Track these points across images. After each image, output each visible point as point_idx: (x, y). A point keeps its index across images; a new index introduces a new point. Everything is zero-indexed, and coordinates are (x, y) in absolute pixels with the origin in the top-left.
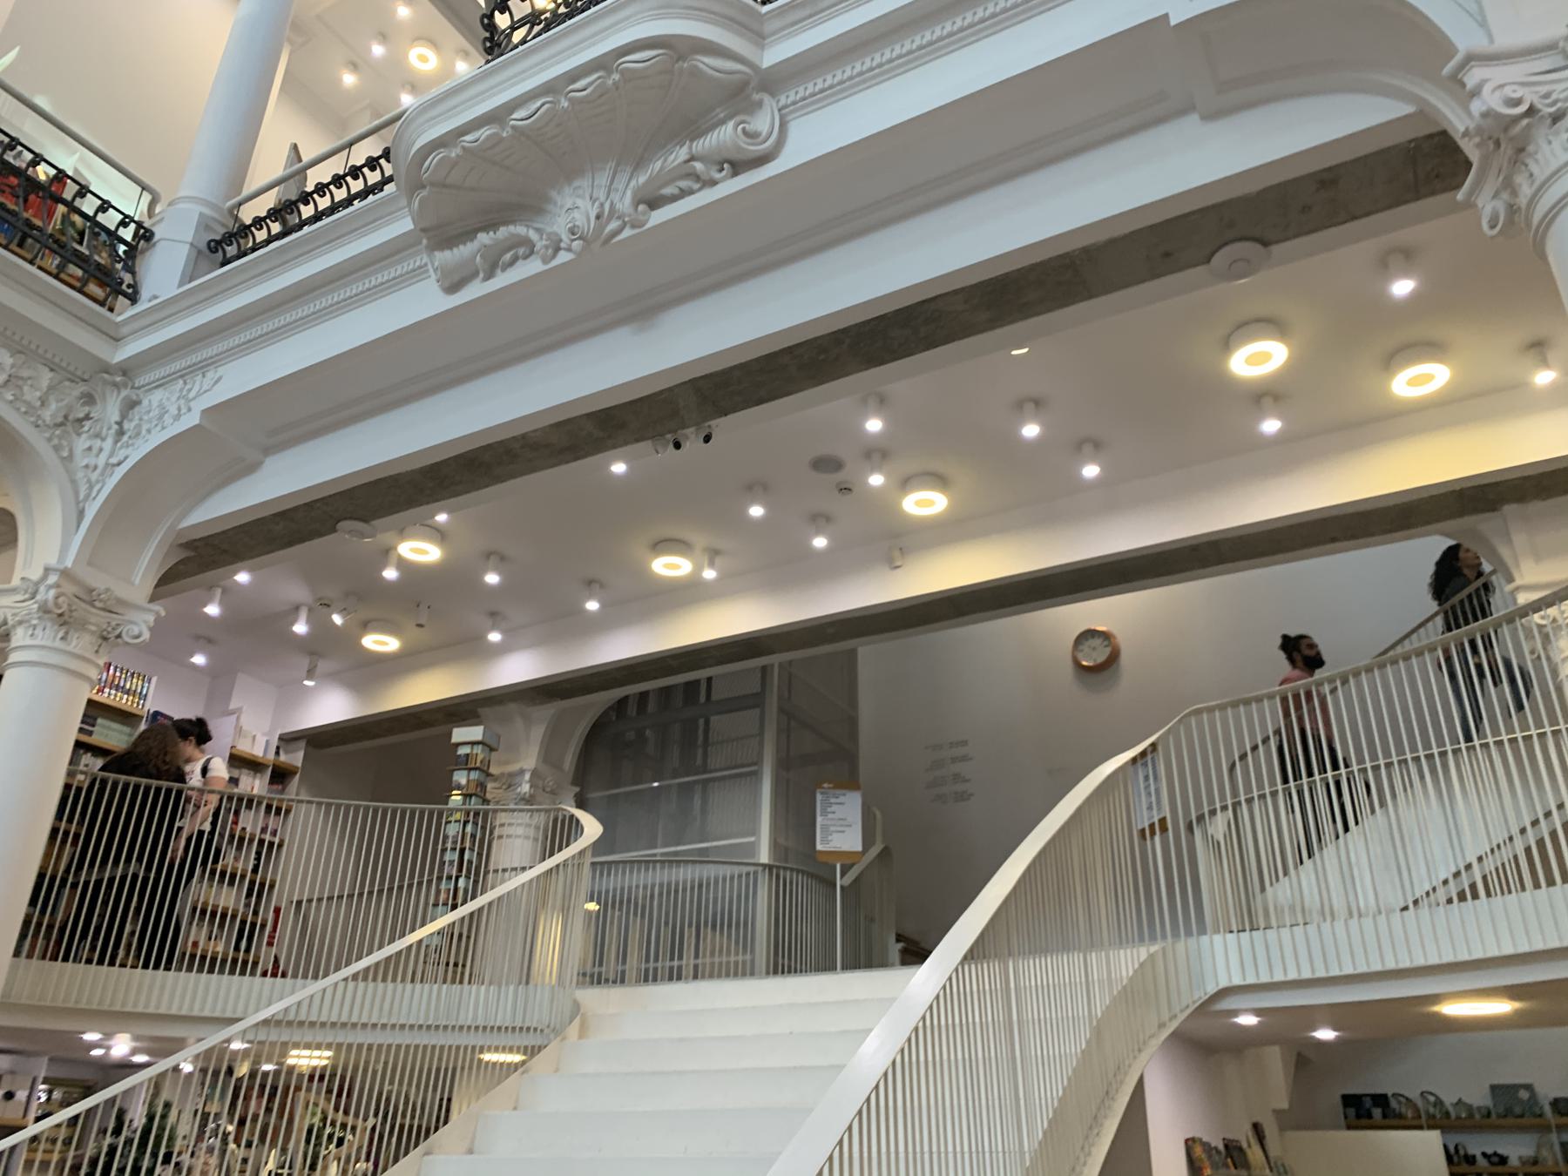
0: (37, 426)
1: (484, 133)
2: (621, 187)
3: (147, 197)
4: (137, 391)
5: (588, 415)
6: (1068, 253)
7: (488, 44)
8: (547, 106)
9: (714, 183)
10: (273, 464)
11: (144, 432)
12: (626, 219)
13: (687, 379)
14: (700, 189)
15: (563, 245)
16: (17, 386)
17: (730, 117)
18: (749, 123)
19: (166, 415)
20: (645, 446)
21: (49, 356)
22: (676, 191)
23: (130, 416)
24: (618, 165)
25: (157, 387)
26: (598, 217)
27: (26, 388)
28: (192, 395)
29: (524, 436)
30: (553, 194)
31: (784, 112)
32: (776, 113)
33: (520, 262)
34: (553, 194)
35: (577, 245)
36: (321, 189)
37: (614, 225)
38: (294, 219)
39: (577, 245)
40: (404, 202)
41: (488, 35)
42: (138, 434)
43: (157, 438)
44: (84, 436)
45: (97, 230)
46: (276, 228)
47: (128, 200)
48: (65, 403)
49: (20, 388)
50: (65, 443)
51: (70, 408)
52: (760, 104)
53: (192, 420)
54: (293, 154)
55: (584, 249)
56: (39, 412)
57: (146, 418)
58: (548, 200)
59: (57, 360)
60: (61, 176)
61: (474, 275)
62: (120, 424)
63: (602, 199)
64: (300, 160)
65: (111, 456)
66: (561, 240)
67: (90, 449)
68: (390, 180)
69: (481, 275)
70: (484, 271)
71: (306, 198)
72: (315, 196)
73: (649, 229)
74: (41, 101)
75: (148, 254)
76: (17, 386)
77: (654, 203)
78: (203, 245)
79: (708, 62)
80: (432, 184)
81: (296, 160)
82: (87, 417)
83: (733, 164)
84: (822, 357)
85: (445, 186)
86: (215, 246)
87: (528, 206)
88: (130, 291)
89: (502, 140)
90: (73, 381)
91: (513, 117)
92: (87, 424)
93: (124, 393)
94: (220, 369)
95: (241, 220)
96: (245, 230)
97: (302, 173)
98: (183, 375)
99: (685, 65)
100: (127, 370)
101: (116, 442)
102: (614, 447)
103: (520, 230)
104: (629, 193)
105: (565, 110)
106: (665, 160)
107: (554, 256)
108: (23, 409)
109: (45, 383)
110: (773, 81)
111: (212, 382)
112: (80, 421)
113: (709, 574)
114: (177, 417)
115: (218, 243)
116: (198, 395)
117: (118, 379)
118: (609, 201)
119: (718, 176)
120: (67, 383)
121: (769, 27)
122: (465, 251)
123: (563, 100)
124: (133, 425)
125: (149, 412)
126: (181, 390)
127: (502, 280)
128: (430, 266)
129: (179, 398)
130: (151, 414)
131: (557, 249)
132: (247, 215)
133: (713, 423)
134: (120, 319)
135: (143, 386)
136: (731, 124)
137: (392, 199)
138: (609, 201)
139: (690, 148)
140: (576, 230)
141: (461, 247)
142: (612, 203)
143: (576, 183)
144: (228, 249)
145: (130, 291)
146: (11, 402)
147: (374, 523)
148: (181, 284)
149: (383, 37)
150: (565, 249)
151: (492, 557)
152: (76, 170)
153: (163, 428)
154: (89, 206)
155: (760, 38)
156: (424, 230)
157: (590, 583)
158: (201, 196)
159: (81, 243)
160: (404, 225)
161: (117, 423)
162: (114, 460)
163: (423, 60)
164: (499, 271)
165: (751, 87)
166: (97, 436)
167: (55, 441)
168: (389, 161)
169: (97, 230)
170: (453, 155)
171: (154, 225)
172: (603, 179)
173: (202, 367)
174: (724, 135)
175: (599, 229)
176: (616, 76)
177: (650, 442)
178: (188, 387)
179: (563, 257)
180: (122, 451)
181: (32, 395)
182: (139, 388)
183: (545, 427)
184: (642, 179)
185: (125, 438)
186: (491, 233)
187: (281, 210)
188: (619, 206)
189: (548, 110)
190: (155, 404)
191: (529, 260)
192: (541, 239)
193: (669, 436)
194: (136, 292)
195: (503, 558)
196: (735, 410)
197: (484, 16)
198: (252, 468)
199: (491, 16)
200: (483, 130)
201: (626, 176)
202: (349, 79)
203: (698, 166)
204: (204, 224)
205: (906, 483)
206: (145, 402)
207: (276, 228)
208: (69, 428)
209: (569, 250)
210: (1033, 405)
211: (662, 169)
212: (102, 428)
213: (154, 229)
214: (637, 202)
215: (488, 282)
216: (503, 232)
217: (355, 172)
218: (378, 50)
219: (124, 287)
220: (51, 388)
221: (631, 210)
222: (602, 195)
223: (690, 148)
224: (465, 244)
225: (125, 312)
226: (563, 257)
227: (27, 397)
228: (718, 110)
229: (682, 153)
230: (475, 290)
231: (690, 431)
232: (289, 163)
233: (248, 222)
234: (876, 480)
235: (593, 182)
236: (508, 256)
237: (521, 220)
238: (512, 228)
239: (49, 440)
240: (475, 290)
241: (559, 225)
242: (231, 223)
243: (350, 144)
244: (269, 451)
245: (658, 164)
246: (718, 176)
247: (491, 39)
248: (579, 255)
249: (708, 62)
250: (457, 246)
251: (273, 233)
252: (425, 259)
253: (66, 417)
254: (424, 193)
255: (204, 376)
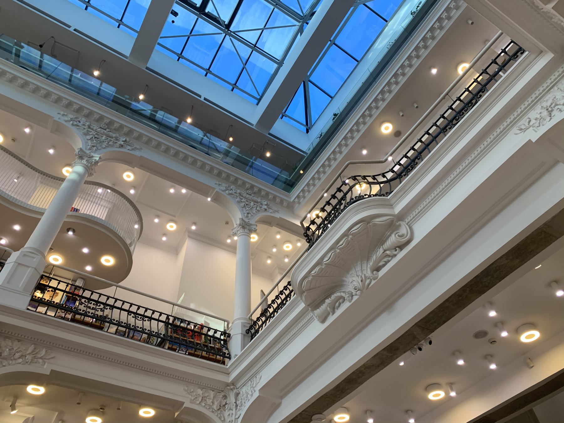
0: (213, 412)
1: (317, 269)
2: (365, 268)
3: (226, 323)
4: (238, 389)
5: (384, 349)
6: (538, 228)
7: (308, 240)
8: (333, 253)
9: (395, 255)
10: (285, 401)
11: (243, 403)
12: (371, 278)
13: (414, 324)
14: (391, 259)
15: (353, 294)
16: (205, 400)
17: (392, 233)
18: (399, 233)
19: (249, 395)
20: (408, 353)
21: (211, 386)
22: (384, 263)
23: (238, 399)
24: (361, 262)
25: (243, 386)
26: (362, 281)
27: (207, 400)
28: (254, 385)
29: (364, 365)
30: (344, 279)
31: (409, 224)
32: (406, 225)
33: (342, 305)
34: (344, 279)
35: (358, 293)
36: (273, 302)
37: (368, 281)
38: (268, 314)
39: (358, 293)
40: (299, 298)
41: (307, 238)
42: (242, 405)
43: (248, 404)
44: (227, 410)
45: (215, 339)
46: (264, 319)
47: (220, 326)
48: (219, 400)
49: (206, 400)
50: (222, 415)
51: (220, 402)
52: (400, 225)
53: (256, 395)
54: (262, 293)
55: (361, 293)
56: (213, 407)
57: (242, 398)
58: (343, 281)
59: (214, 387)
60: (202, 327)
61: (329, 314)
62: (236, 403)
63: (361, 275)
64: (265, 295)
65: (236, 415)
66: (352, 293)
67: (229, 415)
68: (292, 291)
69: (331, 314)
70: (331, 312)
71: (269, 306)
72: (272, 304)
73: (380, 278)
74: (192, 306)
75: (230, 341)
76: (205, 400)
77: (378, 269)
78: (245, 333)
79: (377, 221)
80: (306, 291)
81: (263, 295)
82: (226, 404)
83: (399, 247)
84: (460, 298)
85: (310, 289)
86: (248, 331)
87: (337, 285)
88: (228, 356)
89: (323, 269)
90: (219, 393)
91: (324, 261)
92: (227, 406)
93: (235, 391)
94: (260, 374)
95: (253, 320)
96: (255, 323)
97: (266, 299)
98: (250, 379)
99: (371, 224)
100: (233, 383)
101: (236, 409)
102: (397, 358)
103: (338, 294)
104: (369, 270)
105: (339, 253)
106: (376, 255)
107: (352, 299)
108: (208, 408)
109: (212, 396)
110: (401, 217)
111: (259, 379)
112: (224, 406)
113: (453, 394)
114: (252, 395)
115: (248, 330)
116: (256, 385)
117: (232, 387)
118: (363, 274)
119: (396, 253)
120: (218, 394)
121: (392, 202)
122: (323, 307)
123: (337, 250)
124: (240, 401)
125: (243, 396)
126: (251, 385)
127: (338, 312)
128: (314, 316)
129: (251, 388)
130: (244, 396)
131: (352, 296)
132: (254, 318)
133: (430, 336)
134: (228, 367)
135: (239, 387)
136: (393, 235)
137: (295, 299)
138: (363, 274)
139: (383, 248)
140: (356, 288)
141: (322, 306)
142: (364, 275)
143: (351, 273)
144: (252, 331)
145: (228, 356)
146: (204, 406)
147: (323, 413)
148: (241, 350)
149: (275, 246)
150: (355, 295)
151: (367, 412)
152: (205, 322)
153: (249, 400)
154: (211, 333)
155: (391, 206)
156: (308, 305)
157: (407, 411)
158: (240, 317)
159: (211, 344)
160: (302, 306)
161: (235, 403)
162: (237, 417)
163: (288, 247)
164: (336, 310)
165: (394, 222)
166: (231, 409)
167: (219, 415)
168: (290, 286)
169: (215, 339)
170: (310, 279)
171: (230, 331)
172: (358, 268)
173: (254, 375)
174: (393, 240)
175: (364, 284)
176: (351, 237)
177: (409, 351)
178: (252, 383)
179: (355, 298)
180: (238, 413)
181: (209, 402)
182: (238, 388)
183: (370, 359)
184: (371, 263)
185: (238, 407)
186: (329, 298)
187: (264, 312)
188: (367, 275)
189: (334, 254)
190: (244, 392)
191: (344, 303)
192: (346, 295)
193: (415, 347)
194: (230, 355)
195: (371, 411)
196: (436, 328)
197: (304, 233)
198: (279, 405)
199: (306, 233)
200: (316, 269)
201: (365, 264)
202: (269, 261)
203: (388, 252)
204: (243, 326)
205: (518, 331)
206: (241, 393)
207: (264, 319)
208: (222, 409)
209: (356, 295)
210: (555, 283)
211: (376, 258)
212: (231, 406)
213: (230, 333)
214: (372, 272)
215: (334, 315)
216: (333, 297)
217: (281, 293)
218: (274, 250)
219: (226, 355)
220: (214, 397)
221: (372, 275)
222: (360, 273)
223: (383, 248)
224: (322, 305)
225: (229, 363)
226: (355, 298)
227: (208, 403)
228: (387, 233)
229: (381, 251)
230: (331, 319)
231: (422, 342)
232: (262, 297)
233: (255, 320)
234: (504, 334)
235: (356, 270)
236: (337, 304)
237: (338, 291)
238: (335, 295)
239: (217, 416)
240: (331, 319)
241: (350, 288)
242: (250, 322)
243: (277, 285)
244: (282, 397)
245: (374, 257)
246: (396, 253)
247: (308, 239)
248: (360, 296)
249: (377, 221)
250: (320, 307)
251: (263, 321)
252: (312, 314)
253: (220, 406)
254: (305, 294)
255: (256, 378)
